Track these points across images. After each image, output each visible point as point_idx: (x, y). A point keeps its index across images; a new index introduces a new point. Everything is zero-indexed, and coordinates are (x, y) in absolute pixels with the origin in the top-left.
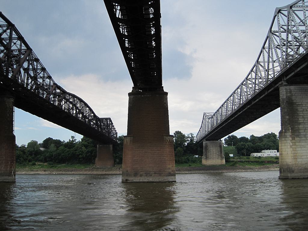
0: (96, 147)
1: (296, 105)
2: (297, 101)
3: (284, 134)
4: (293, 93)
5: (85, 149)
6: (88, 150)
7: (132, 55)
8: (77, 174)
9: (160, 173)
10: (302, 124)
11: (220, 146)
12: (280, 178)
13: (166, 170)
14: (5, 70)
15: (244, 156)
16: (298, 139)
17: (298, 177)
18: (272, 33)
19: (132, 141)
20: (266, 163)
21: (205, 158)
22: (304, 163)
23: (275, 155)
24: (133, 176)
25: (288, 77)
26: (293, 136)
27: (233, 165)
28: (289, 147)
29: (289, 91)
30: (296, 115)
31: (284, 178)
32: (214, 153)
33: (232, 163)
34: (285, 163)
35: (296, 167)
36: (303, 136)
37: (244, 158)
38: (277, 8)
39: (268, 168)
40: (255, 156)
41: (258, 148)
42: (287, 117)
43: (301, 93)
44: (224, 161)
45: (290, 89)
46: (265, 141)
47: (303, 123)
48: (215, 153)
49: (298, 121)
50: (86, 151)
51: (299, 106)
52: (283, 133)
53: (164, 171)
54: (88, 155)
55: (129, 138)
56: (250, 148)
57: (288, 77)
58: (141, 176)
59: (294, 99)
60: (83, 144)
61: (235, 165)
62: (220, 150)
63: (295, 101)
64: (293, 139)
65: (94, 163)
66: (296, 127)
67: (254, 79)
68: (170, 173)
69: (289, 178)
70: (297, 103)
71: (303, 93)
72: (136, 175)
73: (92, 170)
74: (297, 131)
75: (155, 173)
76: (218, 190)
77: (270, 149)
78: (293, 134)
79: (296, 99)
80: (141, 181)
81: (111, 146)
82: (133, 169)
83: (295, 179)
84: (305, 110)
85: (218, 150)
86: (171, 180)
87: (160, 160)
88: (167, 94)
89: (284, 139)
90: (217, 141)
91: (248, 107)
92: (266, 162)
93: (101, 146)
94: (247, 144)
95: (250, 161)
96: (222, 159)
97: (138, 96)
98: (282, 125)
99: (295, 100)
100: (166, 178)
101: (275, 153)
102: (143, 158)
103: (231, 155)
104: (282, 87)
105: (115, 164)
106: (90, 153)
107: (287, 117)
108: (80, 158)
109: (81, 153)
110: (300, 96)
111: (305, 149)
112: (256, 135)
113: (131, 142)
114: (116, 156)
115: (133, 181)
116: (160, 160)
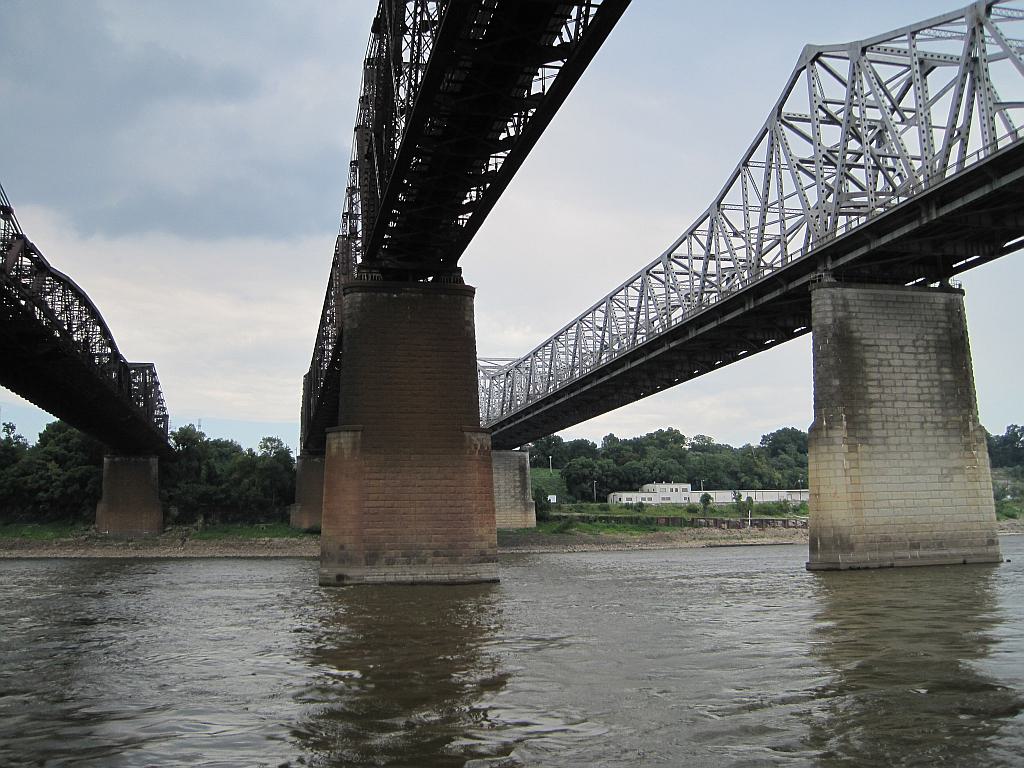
0: (100, 463)
1: (860, 347)
2: (864, 335)
3: (824, 433)
4: (852, 309)
5: (60, 471)
6: (69, 473)
8: (31, 559)
9: (452, 554)
10: (875, 404)
12: (813, 567)
13: (471, 544)
14: (393, 218)
15: (592, 501)
16: (866, 448)
17: (864, 565)
18: (783, 122)
20: (661, 525)
22: (881, 521)
23: (685, 499)
24: (363, 561)
25: (842, 261)
26: (852, 440)
27: (561, 531)
28: (839, 473)
29: (841, 302)
30: (861, 375)
31: (825, 566)
32: (502, 490)
33: (558, 525)
35: (860, 533)
36: (878, 441)
37: (593, 509)
38: (808, 47)
39: (669, 539)
40: (624, 501)
41: (632, 476)
42: (836, 382)
43: (873, 311)
44: (532, 516)
45: (844, 299)
46: (653, 454)
47: (880, 401)
48: (505, 491)
49: (866, 397)
50: (62, 478)
51: (868, 351)
52: (821, 429)
53: (466, 546)
54: (69, 491)
55: (350, 434)
56: (606, 476)
57: (842, 261)
58: (390, 562)
59: (854, 328)
60: (50, 453)
61: (568, 531)
62: (520, 481)
64: (853, 448)
65: (91, 520)
66: (860, 414)
67: (701, 258)
68: (483, 554)
69: (842, 567)
70: (863, 342)
71: (880, 310)
72: (372, 559)
73: (88, 545)
74: (863, 426)
75: (436, 554)
77: (668, 482)
78: (852, 433)
79: (860, 328)
80: (391, 579)
81: (154, 461)
82: (364, 541)
83: (859, 569)
84: (885, 363)
85: (515, 481)
86: (487, 576)
88: (471, 291)
89: (826, 447)
90: (509, 452)
91: (673, 345)
92: (660, 521)
93: (117, 459)
94: (599, 462)
95: (612, 518)
96: (526, 510)
97: (379, 295)
98: (819, 405)
99: (859, 331)
100: (470, 569)
101: (686, 494)
102: (396, 504)
103: (553, 499)
104: (822, 290)
105: (165, 524)
106: (76, 486)
107: (836, 382)
108: (40, 503)
109: (45, 484)
110: (873, 319)
111: (884, 479)
112: (621, 435)
113: (354, 448)
114: (170, 497)
115: (363, 581)
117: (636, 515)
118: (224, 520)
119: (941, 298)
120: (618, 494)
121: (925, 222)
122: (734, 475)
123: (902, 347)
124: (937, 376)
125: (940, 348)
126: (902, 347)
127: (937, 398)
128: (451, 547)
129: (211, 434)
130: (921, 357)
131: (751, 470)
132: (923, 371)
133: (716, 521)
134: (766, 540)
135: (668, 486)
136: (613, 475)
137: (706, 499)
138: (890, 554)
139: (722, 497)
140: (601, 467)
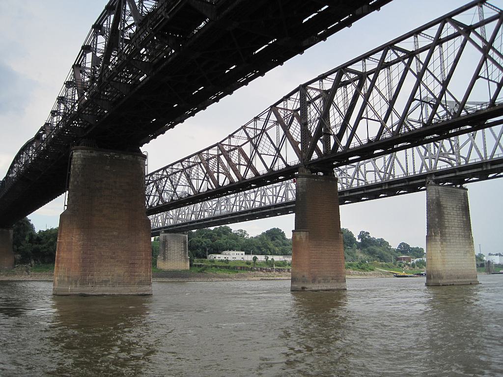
7: (395, 147)
11: (184, 241)
19: (308, 237)
21: (163, 259)
27: (201, 272)
28: (439, 252)
34: (435, 269)
39: (245, 277)
52: (432, 236)
58: (319, 282)
59: (441, 200)
63: (442, 203)
64: (442, 243)
75: (332, 279)
76: (20, 330)
80: (320, 288)
82: (311, 274)
85: (181, 248)
87: (337, 262)
88: (145, 157)
94: (204, 240)
101: (242, 256)
102: (320, 260)
107: (437, 220)
111: (450, 254)
113: (306, 238)
116: (337, 262)
117: (226, 265)
118: (43, 262)
119: (462, 191)
120: (214, 255)
121: (485, 169)
122: (259, 248)
123: (453, 208)
124: (462, 219)
125: (463, 210)
126: (453, 208)
127: (462, 226)
128: (337, 276)
129: (31, 222)
130: (458, 212)
131: (266, 246)
132: (459, 217)
133: (261, 268)
134: (283, 278)
135: (235, 252)
136: (210, 246)
137: (255, 259)
138: (452, 281)
139: (261, 258)
140: (205, 242)
